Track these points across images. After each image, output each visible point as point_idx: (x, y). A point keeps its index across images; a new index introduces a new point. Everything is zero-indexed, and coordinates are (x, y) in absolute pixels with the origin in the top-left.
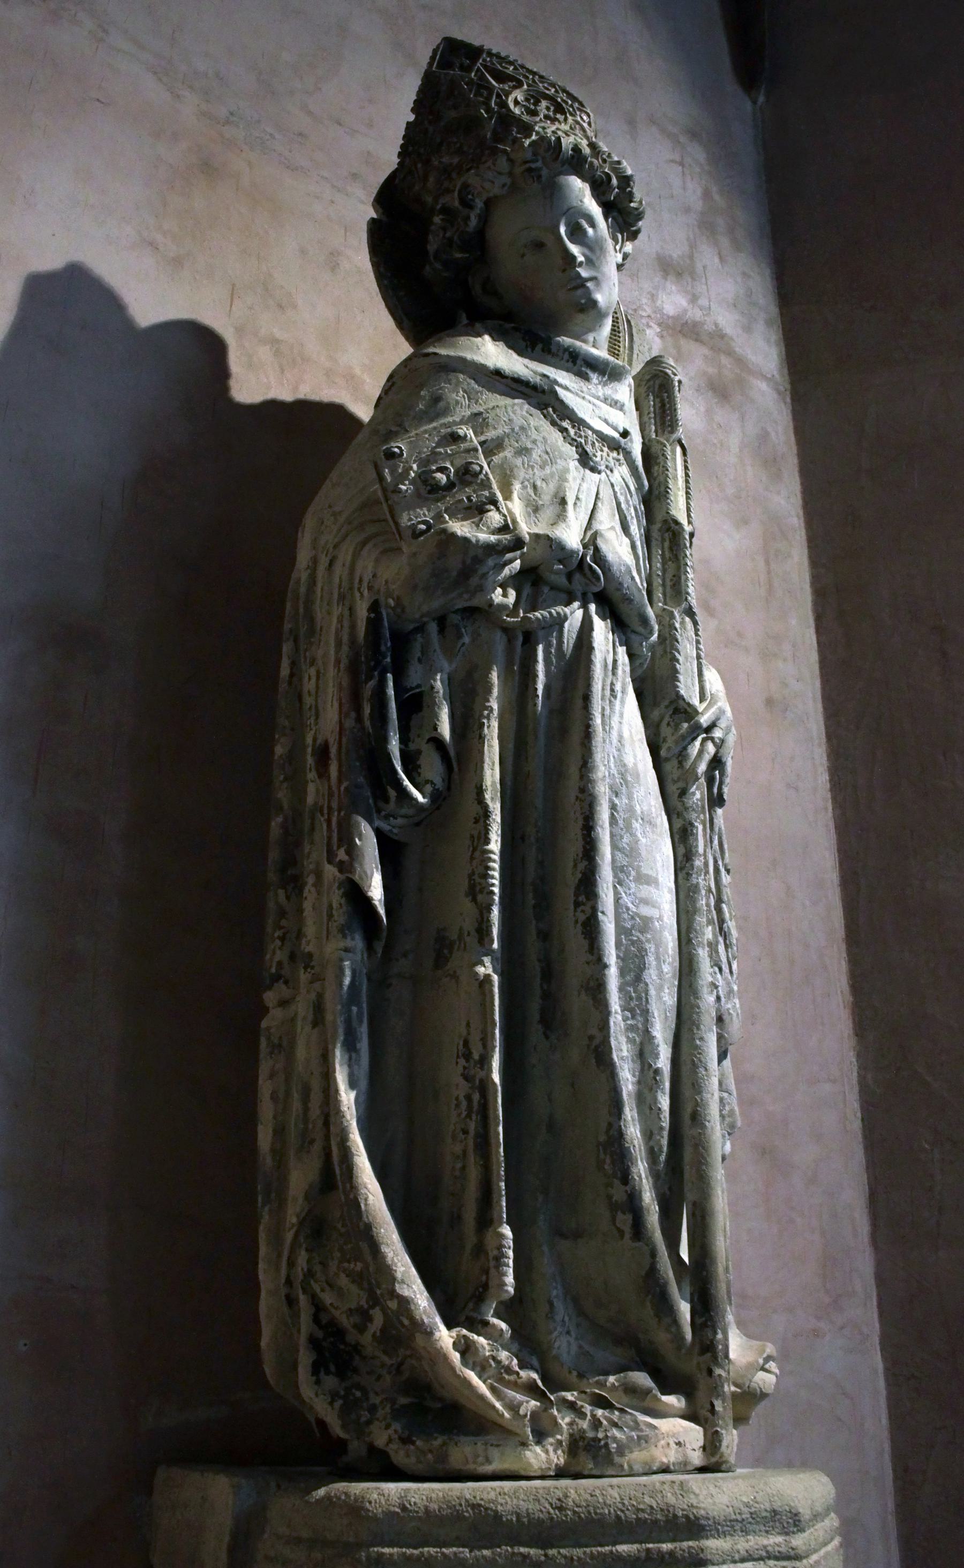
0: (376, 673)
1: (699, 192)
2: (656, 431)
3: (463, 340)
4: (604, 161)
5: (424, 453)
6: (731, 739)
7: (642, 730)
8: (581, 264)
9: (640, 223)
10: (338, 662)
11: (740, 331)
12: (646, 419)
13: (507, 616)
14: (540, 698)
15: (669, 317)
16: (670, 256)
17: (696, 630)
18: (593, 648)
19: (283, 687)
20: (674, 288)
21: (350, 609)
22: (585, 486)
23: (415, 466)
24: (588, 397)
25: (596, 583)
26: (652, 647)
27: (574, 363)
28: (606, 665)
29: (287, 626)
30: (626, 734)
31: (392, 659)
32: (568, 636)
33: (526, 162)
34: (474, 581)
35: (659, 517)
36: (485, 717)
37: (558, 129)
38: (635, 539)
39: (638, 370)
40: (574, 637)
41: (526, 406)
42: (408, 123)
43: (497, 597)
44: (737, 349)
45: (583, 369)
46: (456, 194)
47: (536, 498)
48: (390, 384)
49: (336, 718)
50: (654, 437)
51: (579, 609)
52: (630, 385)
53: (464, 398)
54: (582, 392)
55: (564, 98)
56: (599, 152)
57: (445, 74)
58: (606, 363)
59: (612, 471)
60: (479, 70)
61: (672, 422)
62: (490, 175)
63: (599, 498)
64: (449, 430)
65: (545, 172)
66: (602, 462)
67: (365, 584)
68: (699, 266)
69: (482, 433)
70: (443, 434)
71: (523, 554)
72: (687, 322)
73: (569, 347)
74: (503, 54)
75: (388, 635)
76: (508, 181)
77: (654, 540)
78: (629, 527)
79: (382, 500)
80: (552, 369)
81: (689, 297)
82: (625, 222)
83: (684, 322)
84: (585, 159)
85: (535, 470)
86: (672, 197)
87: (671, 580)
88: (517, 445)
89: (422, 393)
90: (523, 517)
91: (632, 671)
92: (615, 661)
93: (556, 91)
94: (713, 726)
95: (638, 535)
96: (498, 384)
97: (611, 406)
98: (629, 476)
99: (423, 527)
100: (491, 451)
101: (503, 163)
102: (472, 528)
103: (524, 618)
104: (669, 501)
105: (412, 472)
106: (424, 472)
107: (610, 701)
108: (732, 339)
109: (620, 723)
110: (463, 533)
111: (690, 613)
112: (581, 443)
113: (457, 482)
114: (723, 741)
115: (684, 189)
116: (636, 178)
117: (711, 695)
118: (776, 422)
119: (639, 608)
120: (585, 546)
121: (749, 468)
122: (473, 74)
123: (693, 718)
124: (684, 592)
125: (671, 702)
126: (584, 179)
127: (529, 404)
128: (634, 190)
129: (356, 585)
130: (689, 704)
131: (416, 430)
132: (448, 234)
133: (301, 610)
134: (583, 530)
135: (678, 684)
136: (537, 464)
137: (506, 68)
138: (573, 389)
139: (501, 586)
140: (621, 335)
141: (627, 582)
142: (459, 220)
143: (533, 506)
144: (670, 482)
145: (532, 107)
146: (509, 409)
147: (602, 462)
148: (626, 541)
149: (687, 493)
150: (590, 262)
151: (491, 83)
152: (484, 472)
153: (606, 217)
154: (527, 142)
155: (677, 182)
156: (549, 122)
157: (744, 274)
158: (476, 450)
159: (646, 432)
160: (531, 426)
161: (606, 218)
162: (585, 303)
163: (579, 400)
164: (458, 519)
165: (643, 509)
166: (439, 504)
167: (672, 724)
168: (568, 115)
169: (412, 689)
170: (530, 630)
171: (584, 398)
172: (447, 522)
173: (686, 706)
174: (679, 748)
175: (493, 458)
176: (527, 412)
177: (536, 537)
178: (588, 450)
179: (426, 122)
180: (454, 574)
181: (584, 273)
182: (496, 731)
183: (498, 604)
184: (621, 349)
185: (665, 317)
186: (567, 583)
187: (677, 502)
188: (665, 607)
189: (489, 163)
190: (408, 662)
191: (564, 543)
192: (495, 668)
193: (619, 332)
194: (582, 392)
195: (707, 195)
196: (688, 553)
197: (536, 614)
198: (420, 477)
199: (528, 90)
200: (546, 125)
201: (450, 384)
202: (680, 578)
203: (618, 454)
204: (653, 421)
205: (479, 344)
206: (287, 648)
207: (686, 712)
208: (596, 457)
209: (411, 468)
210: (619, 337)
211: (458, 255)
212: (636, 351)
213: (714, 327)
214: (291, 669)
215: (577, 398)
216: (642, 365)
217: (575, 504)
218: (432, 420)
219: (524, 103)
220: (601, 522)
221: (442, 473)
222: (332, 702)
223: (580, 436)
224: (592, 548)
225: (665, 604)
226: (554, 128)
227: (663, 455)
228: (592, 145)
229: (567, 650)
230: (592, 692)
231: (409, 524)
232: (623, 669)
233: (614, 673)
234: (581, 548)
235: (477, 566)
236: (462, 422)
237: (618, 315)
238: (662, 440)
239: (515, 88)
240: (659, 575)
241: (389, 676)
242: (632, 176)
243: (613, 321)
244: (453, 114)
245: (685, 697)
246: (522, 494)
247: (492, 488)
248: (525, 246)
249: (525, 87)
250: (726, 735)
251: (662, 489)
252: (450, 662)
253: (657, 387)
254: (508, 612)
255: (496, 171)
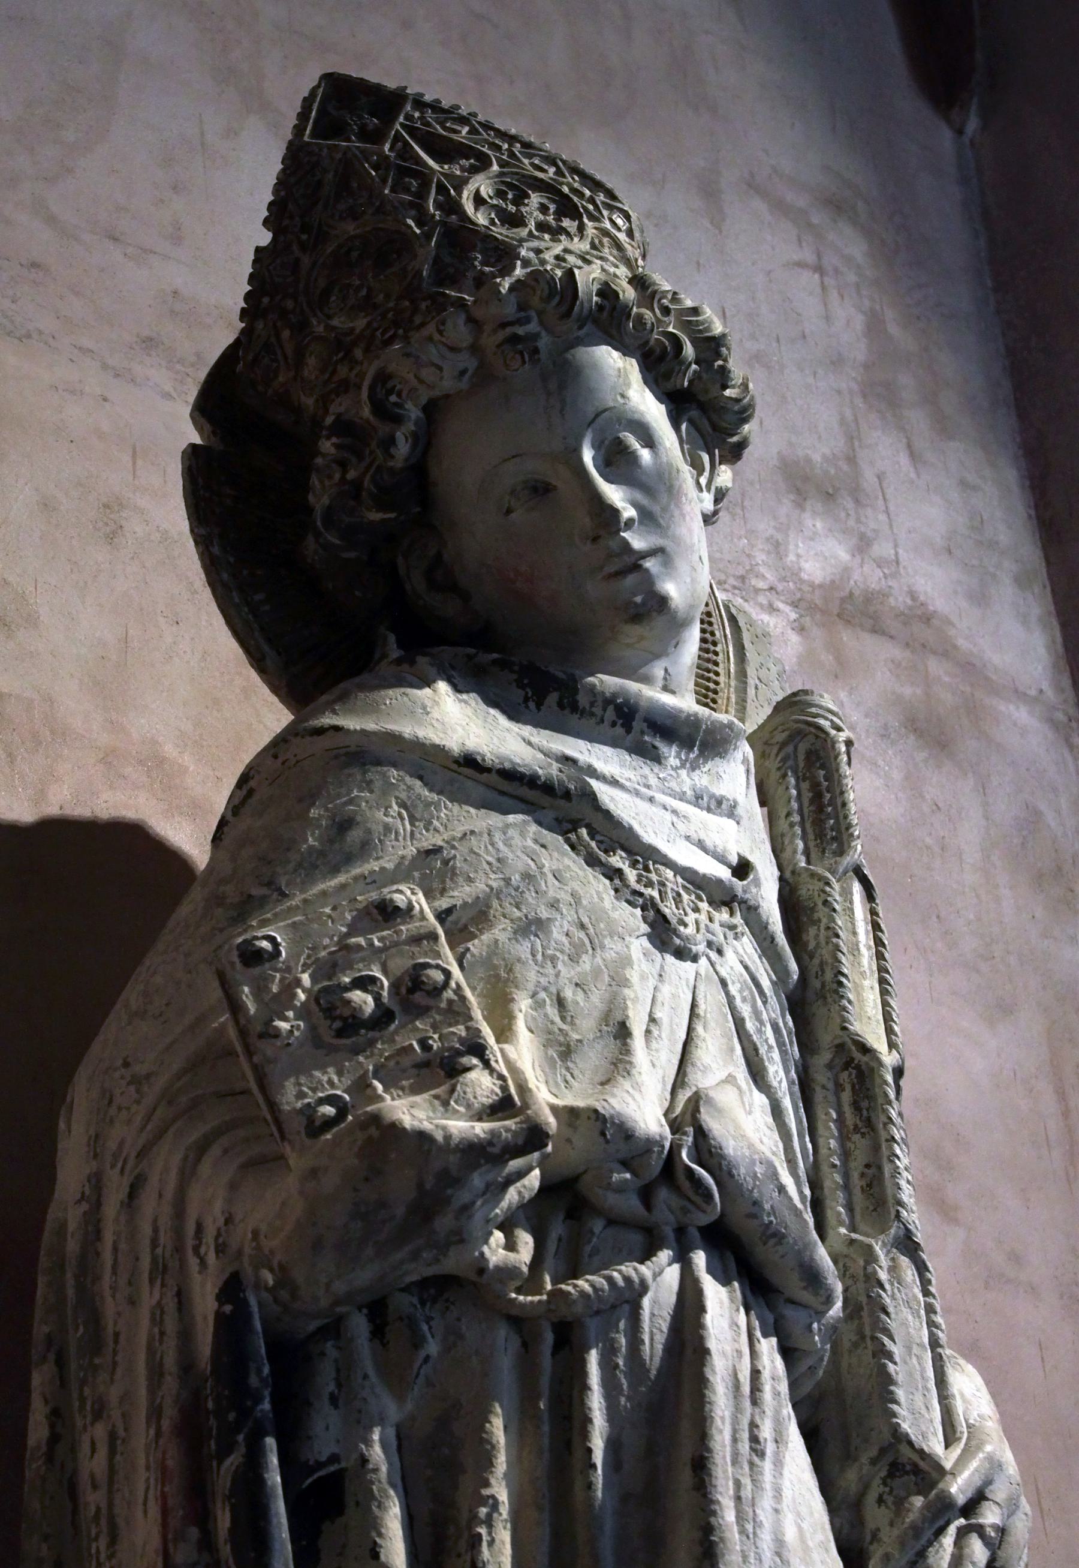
0: (241, 1438)
1: (859, 322)
2: (807, 853)
3: (393, 696)
4: (666, 311)
5: (325, 948)
6: (1021, 1527)
7: (825, 1519)
8: (629, 523)
9: (746, 427)
10: (155, 1413)
11: (964, 604)
12: (783, 825)
13: (519, 1291)
14: (600, 1471)
15: (812, 585)
16: (808, 460)
17: (925, 1283)
18: (707, 1352)
19: (34, 1467)
20: (819, 525)
21: (179, 1294)
22: (666, 990)
23: (306, 979)
24: (660, 797)
25: (704, 1205)
26: (833, 1332)
27: (628, 729)
28: (737, 1385)
29: (41, 1329)
30: (790, 1534)
31: (273, 1402)
32: (651, 1327)
33: (504, 325)
34: (444, 1223)
35: (826, 1038)
36: (482, 1522)
37: (566, 251)
38: (780, 1094)
39: (761, 722)
40: (665, 1329)
41: (533, 828)
42: (258, 250)
43: (494, 1252)
44: (961, 642)
45: (646, 738)
46: (365, 393)
47: (564, 1027)
48: (244, 792)
49: (156, 1541)
50: (803, 864)
51: (670, 1265)
52: (745, 761)
53: (402, 819)
54: (648, 787)
55: (576, 185)
56: (655, 292)
57: (329, 147)
58: (694, 722)
59: (720, 952)
60: (398, 137)
61: (839, 832)
62: (433, 353)
63: (698, 1016)
64: (374, 896)
65: (544, 342)
66: (699, 937)
67: (209, 1238)
68: (869, 476)
69: (443, 891)
70: (360, 906)
71: (545, 1157)
72: (851, 594)
73: (615, 695)
74: (445, 104)
75: (263, 1351)
76: (470, 363)
77: (818, 1089)
78: (764, 1069)
79: (239, 1049)
80: (582, 744)
81: (854, 541)
82: (715, 427)
83: (846, 593)
84: (626, 310)
85: (560, 966)
86: (804, 337)
87: (862, 1175)
88: (517, 914)
89: (314, 813)
90: (539, 1072)
91: (793, 1386)
92: (756, 1373)
93: (559, 172)
94: (978, 1498)
95: (785, 1084)
96: (469, 783)
97: (709, 810)
98: (756, 957)
99: (329, 1110)
100: (466, 927)
101: (458, 330)
102: (434, 1111)
103: (555, 1294)
104: (845, 1002)
105: (299, 991)
106: (325, 990)
107: (752, 1464)
108: (950, 623)
109: (777, 1511)
110: (416, 1123)
111: (908, 1245)
112: (652, 898)
113: (396, 1008)
114: (1002, 1531)
115: (828, 318)
116: (733, 340)
117: (969, 1426)
118: (1055, 790)
119: (799, 1252)
120: (675, 1126)
121: (1006, 892)
122: (387, 147)
123: (933, 1484)
124: (891, 1201)
125: (883, 1451)
126: (625, 350)
127: (540, 823)
128: (732, 364)
129: (190, 1242)
130: (921, 1452)
131: (302, 891)
132: (351, 475)
133: (71, 1292)
134: (669, 1087)
135: (895, 1407)
136: (562, 952)
137: (455, 132)
138: (628, 784)
139: (500, 1228)
140: (718, 649)
141: (769, 1199)
142: (374, 444)
143: (561, 1045)
144: (843, 960)
145: (512, 208)
146: (498, 837)
147: (699, 937)
148: (760, 1100)
149: (882, 981)
150: (647, 518)
151: (425, 164)
152: (453, 985)
153: (675, 421)
154: (506, 284)
155: (809, 305)
156: (547, 237)
157: (964, 484)
158: (433, 937)
159: (786, 855)
160: (546, 870)
161: (676, 425)
162: (644, 603)
163: (644, 805)
164: (403, 1089)
165: (791, 1023)
166: (361, 1059)
167: (890, 1500)
168: (586, 220)
169: (320, 1465)
170: (570, 1319)
171: (651, 800)
172: (380, 1099)
173: (915, 1458)
174: (910, 1555)
175: (470, 945)
176: (536, 841)
177: (569, 1115)
178: (667, 911)
179: (295, 248)
180: (400, 1211)
181: (637, 542)
182: (508, 1550)
183: (498, 1269)
184: (722, 679)
185: (806, 588)
186: (646, 1213)
187: (861, 1000)
188: (854, 1236)
189: (431, 329)
190: (309, 1404)
191: (630, 1124)
192: (499, 1410)
193: (715, 644)
194: (648, 787)
195: (874, 326)
196: (893, 1114)
197: (580, 1282)
198: (317, 1001)
199: (501, 174)
200: (542, 245)
201: (371, 792)
202: (880, 1168)
203: (732, 914)
204: (798, 830)
205: (429, 703)
206: (39, 1379)
207: (916, 1470)
208: (686, 925)
209: (298, 983)
210: (716, 654)
211: (375, 516)
212: (752, 681)
213: (909, 602)
214: (52, 1426)
215: (638, 801)
216: (768, 710)
217: (648, 1032)
218: (335, 870)
219: (495, 202)
220: (706, 1069)
221: (365, 990)
222: (145, 1503)
223: (649, 884)
224: (690, 1130)
225: (853, 1228)
226: (558, 249)
227: (826, 903)
228: (639, 282)
229: (651, 1359)
230: (709, 1450)
231: (299, 1105)
232: (774, 1388)
233: (755, 1402)
234: (667, 1131)
235: (449, 1191)
236: (401, 874)
237: (711, 608)
238: (820, 870)
239: (474, 170)
240: (834, 1166)
241: (270, 1442)
242: (724, 335)
243: (703, 631)
244: (350, 228)
245: (913, 1438)
246: (534, 1019)
247: (471, 1019)
248: (513, 492)
249: (495, 167)
250: (1009, 1517)
251: (829, 975)
252: (400, 1398)
253: (801, 757)
254: (518, 1283)
255: (445, 345)
